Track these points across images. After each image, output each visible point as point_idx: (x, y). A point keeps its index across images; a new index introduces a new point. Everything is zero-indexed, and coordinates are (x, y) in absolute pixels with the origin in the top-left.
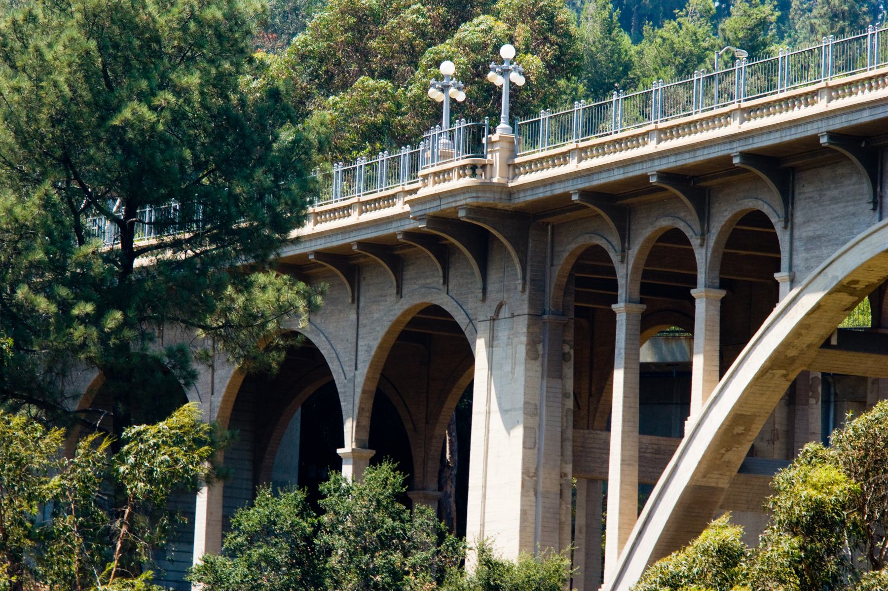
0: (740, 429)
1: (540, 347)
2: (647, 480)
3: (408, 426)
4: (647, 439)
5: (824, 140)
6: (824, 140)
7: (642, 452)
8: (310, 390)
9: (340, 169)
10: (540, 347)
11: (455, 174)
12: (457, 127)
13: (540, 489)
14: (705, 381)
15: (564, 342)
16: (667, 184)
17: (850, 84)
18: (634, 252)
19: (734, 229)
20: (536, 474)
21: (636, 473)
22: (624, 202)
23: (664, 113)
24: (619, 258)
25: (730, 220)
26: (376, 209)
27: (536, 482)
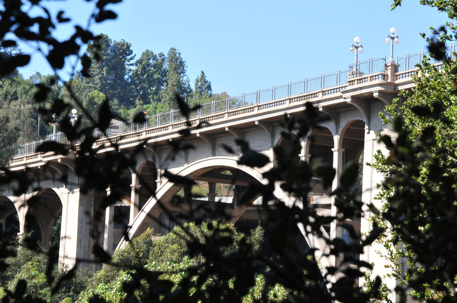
0: (144, 227)
1: (83, 202)
2: (115, 243)
3: (40, 226)
4: (116, 230)
5: (227, 129)
6: (227, 129)
7: (114, 233)
8: (8, 214)
9: (173, 112)
10: (83, 202)
11: (356, 82)
12: (58, 134)
13: (82, 246)
14: (134, 212)
15: (91, 200)
16: (233, 131)
17: (179, 124)
18: (340, 130)
19: (348, 128)
20: (81, 241)
21: (112, 240)
22: (188, 142)
23: (161, 123)
24: (335, 132)
25: (142, 164)
26: (131, 137)
27: (81, 243)
